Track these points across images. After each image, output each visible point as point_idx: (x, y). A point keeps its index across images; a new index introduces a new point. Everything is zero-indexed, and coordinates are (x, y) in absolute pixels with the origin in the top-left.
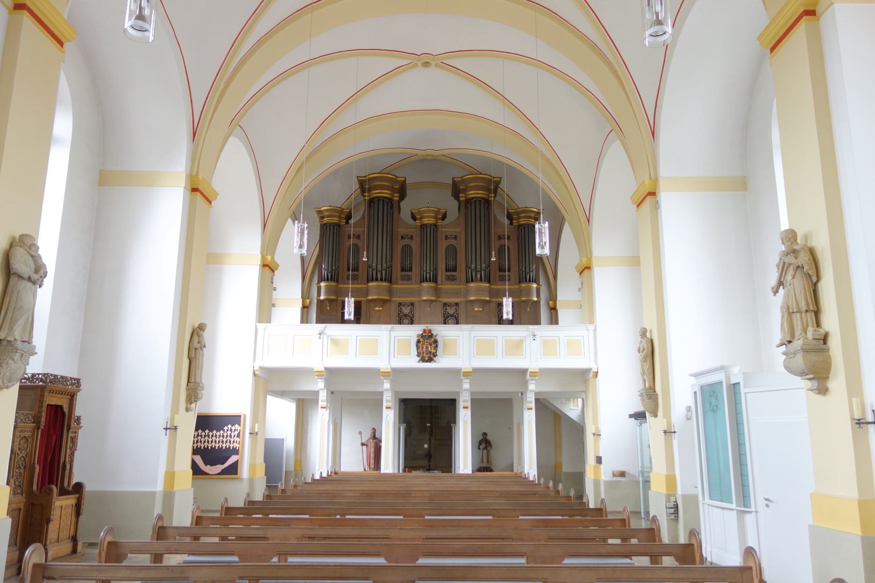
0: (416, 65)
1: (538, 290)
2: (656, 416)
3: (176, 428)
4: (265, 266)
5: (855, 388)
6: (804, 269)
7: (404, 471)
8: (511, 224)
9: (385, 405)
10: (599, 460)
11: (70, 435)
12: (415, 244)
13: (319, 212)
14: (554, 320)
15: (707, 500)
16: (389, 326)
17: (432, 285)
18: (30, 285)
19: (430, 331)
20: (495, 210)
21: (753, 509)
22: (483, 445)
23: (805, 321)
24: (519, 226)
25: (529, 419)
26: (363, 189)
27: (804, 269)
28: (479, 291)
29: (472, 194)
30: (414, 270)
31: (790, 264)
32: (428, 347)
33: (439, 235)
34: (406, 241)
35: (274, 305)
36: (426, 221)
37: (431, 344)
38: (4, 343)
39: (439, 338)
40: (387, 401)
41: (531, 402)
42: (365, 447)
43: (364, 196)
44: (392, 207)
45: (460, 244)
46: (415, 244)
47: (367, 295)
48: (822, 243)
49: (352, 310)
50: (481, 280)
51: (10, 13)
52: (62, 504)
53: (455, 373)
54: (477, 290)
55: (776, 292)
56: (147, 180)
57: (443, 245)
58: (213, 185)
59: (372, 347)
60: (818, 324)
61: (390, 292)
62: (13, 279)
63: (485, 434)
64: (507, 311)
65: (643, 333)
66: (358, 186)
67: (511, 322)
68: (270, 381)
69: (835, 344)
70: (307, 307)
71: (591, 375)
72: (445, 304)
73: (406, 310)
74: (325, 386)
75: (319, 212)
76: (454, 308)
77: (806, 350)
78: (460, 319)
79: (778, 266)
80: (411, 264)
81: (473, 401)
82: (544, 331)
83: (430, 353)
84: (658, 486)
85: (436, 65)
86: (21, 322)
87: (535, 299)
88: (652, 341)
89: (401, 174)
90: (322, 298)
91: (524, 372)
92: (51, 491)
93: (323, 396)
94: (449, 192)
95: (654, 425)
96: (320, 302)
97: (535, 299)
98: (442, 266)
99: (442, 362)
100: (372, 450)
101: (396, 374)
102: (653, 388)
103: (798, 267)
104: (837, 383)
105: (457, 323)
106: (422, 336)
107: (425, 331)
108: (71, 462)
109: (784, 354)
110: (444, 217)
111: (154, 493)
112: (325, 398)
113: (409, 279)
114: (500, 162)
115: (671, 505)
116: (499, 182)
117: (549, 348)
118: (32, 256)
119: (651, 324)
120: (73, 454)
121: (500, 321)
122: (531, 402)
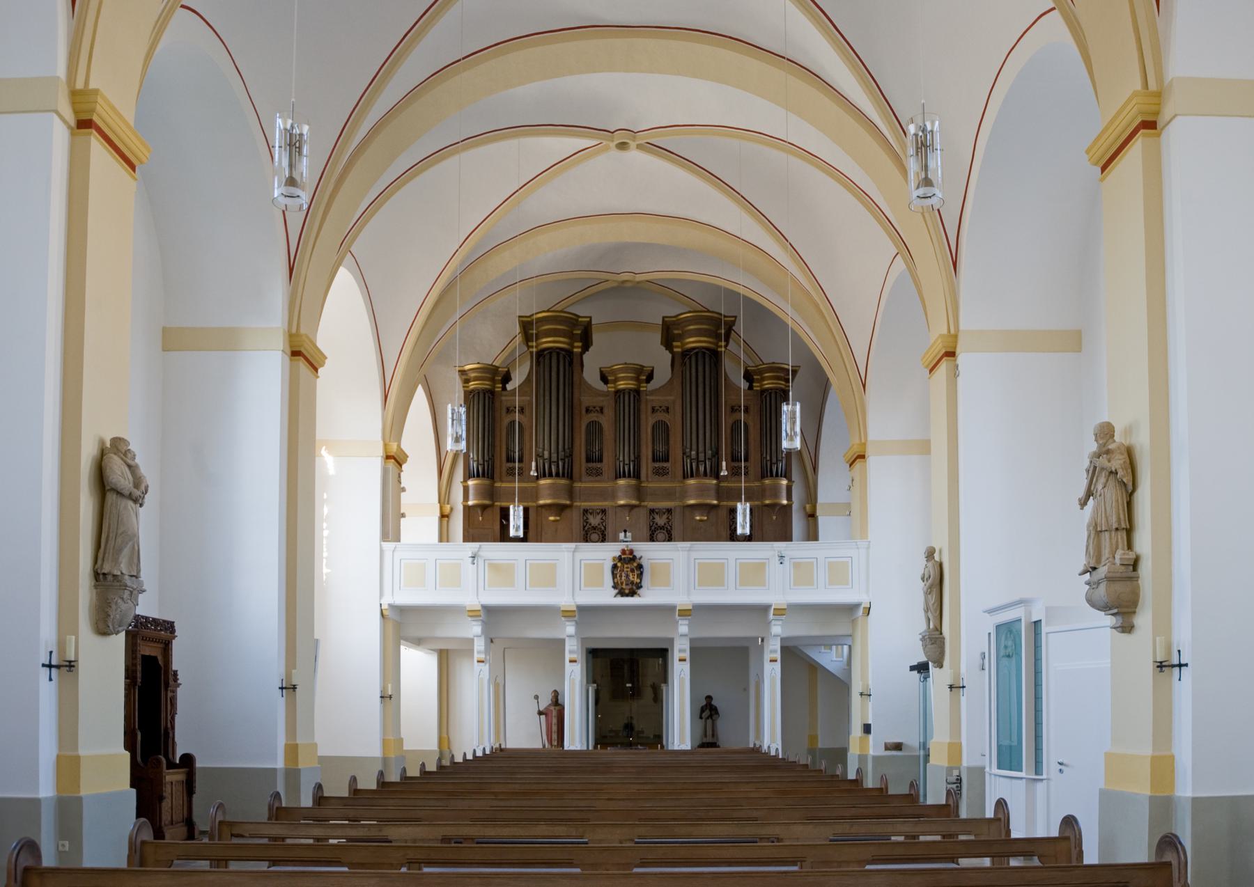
0: (607, 148)
1: (789, 489)
2: (941, 667)
3: (294, 688)
4: (388, 457)
5: (1164, 624)
6: (1117, 478)
7: (595, 747)
8: (751, 388)
9: (568, 657)
10: (867, 729)
11: (170, 694)
12: (606, 421)
13: (462, 372)
14: (812, 534)
15: (996, 771)
16: (573, 545)
17: (633, 482)
18: (130, 503)
19: (631, 552)
20: (727, 365)
21: (1044, 776)
22: (707, 713)
23: (1114, 541)
24: (763, 391)
25: (772, 673)
26: (527, 338)
27: (1117, 478)
28: (702, 491)
29: (692, 342)
30: (605, 460)
31: (1103, 469)
32: (628, 575)
33: (643, 407)
34: (593, 417)
35: (403, 515)
36: (622, 385)
37: (632, 571)
38: (110, 578)
39: (643, 562)
40: (571, 652)
41: (775, 651)
42: (543, 717)
43: (529, 347)
44: (571, 363)
45: (674, 420)
46: (606, 421)
47: (537, 499)
48: (1142, 441)
49: (521, 523)
50: (705, 474)
51: (72, 134)
52: (173, 778)
53: (666, 611)
54: (696, 491)
55: (1083, 503)
56: (227, 340)
57: (648, 421)
58: (319, 344)
59: (546, 576)
60: (1130, 546)
61: (571, 493)
62: (111, 497)
63: (709, 698)
64: (743, 527)
65: (930, 554)
66: (518, 329)
67: (749, 538)
68: (402, 624)
69: (1145, 569)
70: (447, 516)
71: (861, 612)
72: (652, 511)
73: (595, 521)
74: (483, 632)
75: (462, 372)
76: (665, 516)
77: (1110, 579)
78: (674, 533)
79: (1088, 471)
80: (601, 450)
81: (693, 650)
82: (796, 549)
83: (632, 583)
84: (938, 759)
85: (639, 147)
86: (126, 551)
87: (785, 502)
88: (941, 565)
89: (582, 311)
90: (470, 503)
91: (763, 609)
92: (159, 762)
93: (479, 645)
94: (658, 337)
95: (939, 678)
96: (468, 510)
97: (785, 502)
98: (647, 453)
99: (649, 596)
100: (555, 721)
101: (585, 613)
102: (939, 629)
103: (1111, 472)
104: (1143, 619)
105: (670, 540)
106: (620, 559)
107: (623, 552)
108: (173, 728)
109: (1088, 583)
110: (650, 377)
111: (275, 770)
112: (482, 648)
113: (598, 473)
114: (732, 291)
115: (953, 779)
116: (733, 323)
117: (803, 574)
118: (129, 466)
119: (941, 543)
120: (173, 718)
121: (733, 537)
122: (775, 651)
